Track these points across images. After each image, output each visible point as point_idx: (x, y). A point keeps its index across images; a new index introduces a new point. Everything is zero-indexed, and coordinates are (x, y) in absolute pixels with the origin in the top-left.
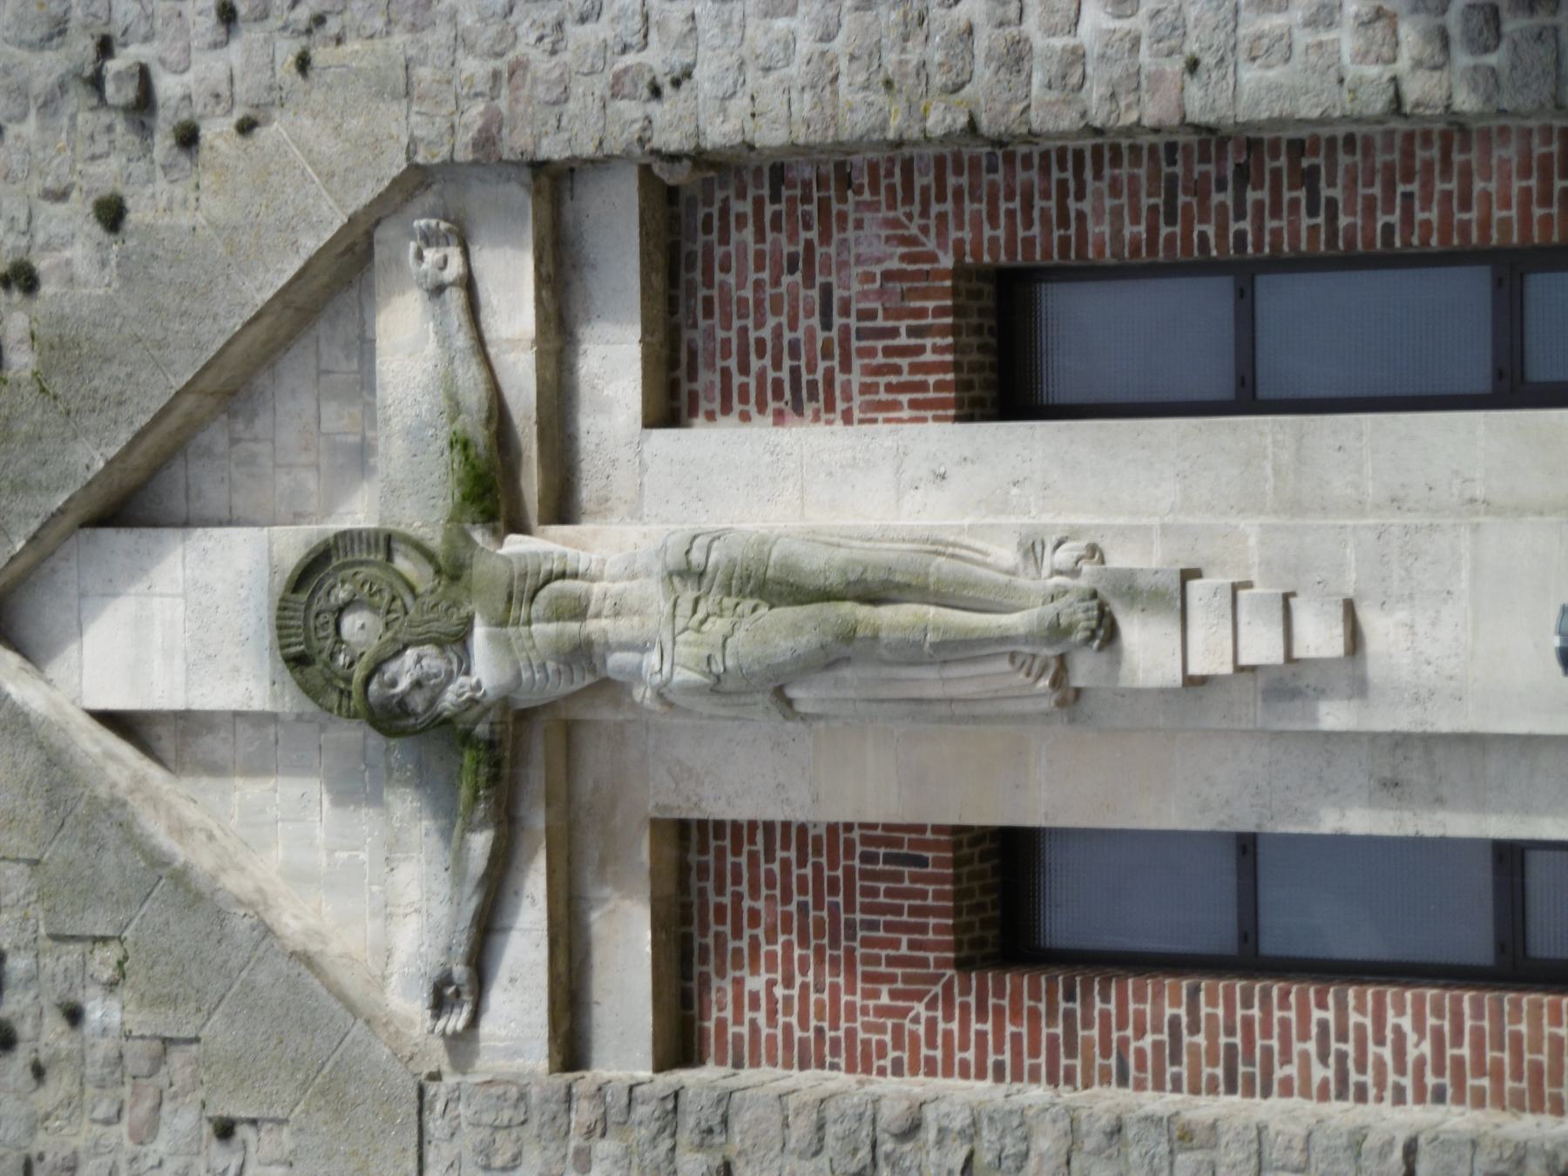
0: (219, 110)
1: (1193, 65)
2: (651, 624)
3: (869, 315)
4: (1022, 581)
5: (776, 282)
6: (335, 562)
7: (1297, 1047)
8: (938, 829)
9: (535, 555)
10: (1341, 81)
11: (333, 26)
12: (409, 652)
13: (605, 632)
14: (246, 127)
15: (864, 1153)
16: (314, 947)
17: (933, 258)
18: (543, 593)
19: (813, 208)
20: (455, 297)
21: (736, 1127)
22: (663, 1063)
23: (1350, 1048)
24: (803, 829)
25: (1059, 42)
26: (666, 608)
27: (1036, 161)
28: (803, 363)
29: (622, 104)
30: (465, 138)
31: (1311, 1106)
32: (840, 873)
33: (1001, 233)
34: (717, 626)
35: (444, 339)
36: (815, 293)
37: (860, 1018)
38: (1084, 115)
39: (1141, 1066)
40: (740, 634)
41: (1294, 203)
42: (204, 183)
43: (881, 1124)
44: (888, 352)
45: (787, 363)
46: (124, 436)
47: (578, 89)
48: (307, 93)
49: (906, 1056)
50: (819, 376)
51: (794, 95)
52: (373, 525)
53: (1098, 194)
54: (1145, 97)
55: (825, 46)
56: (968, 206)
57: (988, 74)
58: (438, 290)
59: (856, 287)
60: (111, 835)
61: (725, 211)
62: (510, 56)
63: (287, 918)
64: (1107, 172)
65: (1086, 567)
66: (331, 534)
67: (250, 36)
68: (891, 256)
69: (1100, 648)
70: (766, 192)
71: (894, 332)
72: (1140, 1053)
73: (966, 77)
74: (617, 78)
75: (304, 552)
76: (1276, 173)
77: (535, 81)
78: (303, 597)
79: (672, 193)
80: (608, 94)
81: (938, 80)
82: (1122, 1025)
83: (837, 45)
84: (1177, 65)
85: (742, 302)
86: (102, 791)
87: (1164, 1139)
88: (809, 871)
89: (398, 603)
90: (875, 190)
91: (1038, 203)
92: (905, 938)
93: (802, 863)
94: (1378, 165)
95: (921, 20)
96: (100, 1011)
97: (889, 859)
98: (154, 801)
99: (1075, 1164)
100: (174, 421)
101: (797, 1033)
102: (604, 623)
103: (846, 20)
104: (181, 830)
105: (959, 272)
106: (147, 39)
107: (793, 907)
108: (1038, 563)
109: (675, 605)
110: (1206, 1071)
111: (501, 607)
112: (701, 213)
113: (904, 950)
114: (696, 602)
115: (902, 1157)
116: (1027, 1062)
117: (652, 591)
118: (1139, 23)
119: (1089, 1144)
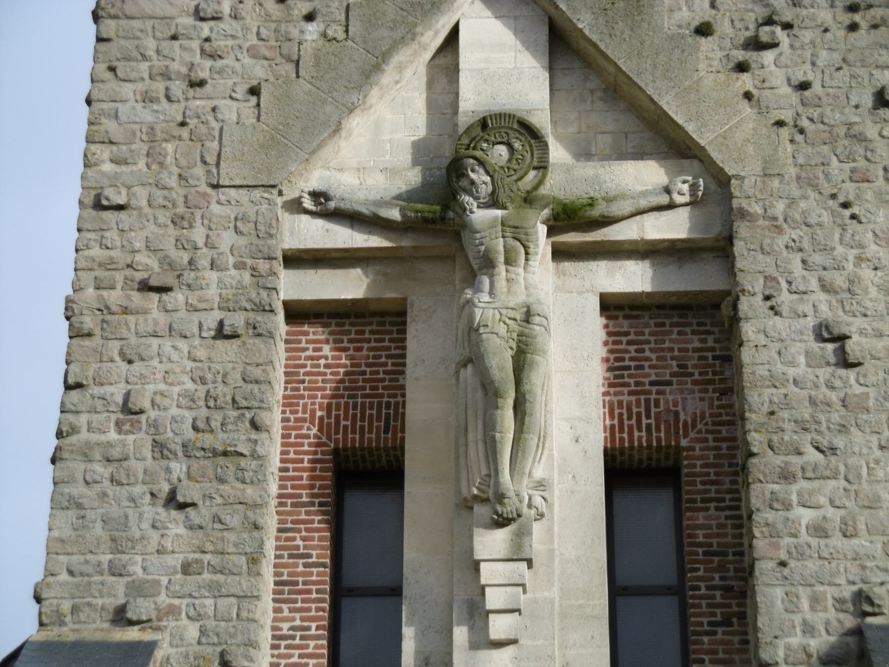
0: (756, 82)
1: (783, 564)
2: (503, 297)
3: (657, 405)
4: (526, 480)
5: (672, 358)
6: (532, 141)
7: (298, 615)
8: (403, 439)
9: (537, 240)
10: (776, 637)
11: (799, 138)
12: (489, 178)
13: (499, 274)
14: (748, 96)
15: (244, 403)
16: (343, 133)
17: (686, 435)
18: (518, 243)
19: (710, 376)
20: (664, 200)
21: (257, 340)
22: (286, 304)
23: (297, 641)
24: (402, 373)
25: (794, 498)
26: (511, 305)
27: (734, 487)
28: (633, 371)
29: (761, 281)
30: (744, 204)
31: (269, 623)
32: (381, 391)
33: (698, 469)
34: (502, 329)
35: (644, 194)
36: (668, 378)
37: (310, 401)
38: (758, 510)
39: (287, 539)
40: (499, 341)
41: (715, 615)
42: (720, 75)
43: (258, 411)
44: (639, 415)
45: (633, 364)
46: (594, 38)
47: (768, 259)
48: (766, 126)
49: (291, 424)
50: (626, 380)
51: (767, 367)
52: (551, 160)
53: (718, 518)
54: (767, 541)
55: (791, 381)
56: (711, 453)
57: (778, 462)
58: (667, 190)
59: (671, 398)
60: (398, 34)
61: (708, 333)
62: (785, 226)
63: (357, 120)
64: (729, 522)
65: (533, 512)
66: (546, 139)
67: (794, 97)
68: (686, 415)
69: (492, 519)
70: (718, 353)
71: (648, 416)
72: (294, 539)
73: (776, 451)
74: (774, 279)
75: (538, 126)
76: (730, 606)
77: (773, 238)
78: (516, 126)
79: (717, 306)
80: (767, 274)
81: (775, 438)
82: (307, 530)
83: (792, 388)
84: (783, 556)
85: (663, 342)
86: (419, 29)
87: (252, 550)
88: (381, 376)
89: (513, 173)
90: (719, 407)
91: (713, 488)
92: (349, 423)
93: (385, 372)
94: (733, 656)
95: (805, 429)
96: (312, 30)
97: (388, 416)
98: (415, 54)
99: (240, 506)
100: (601, 61)
101: (302, 371)
102: (504, 273)
103: (804, 392)
104: (401, 68)
105: (678, 447)
106: (792, 46)
107: (363, 368)
108: (535, 488)
109: (512, 309)
110: (285, 571)
111: (511, 223)
112: (708, 321)
113: (343, 423)
114: (515, 320)
115: (243, 422)
116: (289, 483)
117: (519, 297)
118: (804, 537)
119: (250, 514)
